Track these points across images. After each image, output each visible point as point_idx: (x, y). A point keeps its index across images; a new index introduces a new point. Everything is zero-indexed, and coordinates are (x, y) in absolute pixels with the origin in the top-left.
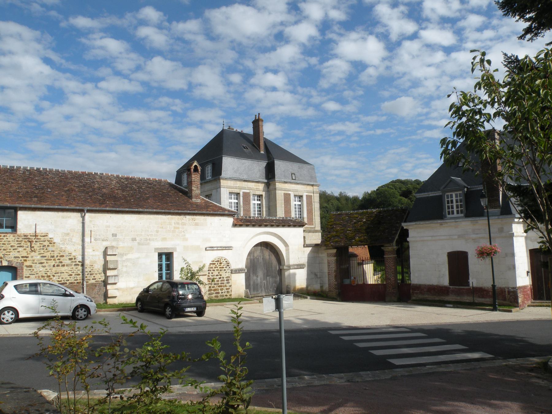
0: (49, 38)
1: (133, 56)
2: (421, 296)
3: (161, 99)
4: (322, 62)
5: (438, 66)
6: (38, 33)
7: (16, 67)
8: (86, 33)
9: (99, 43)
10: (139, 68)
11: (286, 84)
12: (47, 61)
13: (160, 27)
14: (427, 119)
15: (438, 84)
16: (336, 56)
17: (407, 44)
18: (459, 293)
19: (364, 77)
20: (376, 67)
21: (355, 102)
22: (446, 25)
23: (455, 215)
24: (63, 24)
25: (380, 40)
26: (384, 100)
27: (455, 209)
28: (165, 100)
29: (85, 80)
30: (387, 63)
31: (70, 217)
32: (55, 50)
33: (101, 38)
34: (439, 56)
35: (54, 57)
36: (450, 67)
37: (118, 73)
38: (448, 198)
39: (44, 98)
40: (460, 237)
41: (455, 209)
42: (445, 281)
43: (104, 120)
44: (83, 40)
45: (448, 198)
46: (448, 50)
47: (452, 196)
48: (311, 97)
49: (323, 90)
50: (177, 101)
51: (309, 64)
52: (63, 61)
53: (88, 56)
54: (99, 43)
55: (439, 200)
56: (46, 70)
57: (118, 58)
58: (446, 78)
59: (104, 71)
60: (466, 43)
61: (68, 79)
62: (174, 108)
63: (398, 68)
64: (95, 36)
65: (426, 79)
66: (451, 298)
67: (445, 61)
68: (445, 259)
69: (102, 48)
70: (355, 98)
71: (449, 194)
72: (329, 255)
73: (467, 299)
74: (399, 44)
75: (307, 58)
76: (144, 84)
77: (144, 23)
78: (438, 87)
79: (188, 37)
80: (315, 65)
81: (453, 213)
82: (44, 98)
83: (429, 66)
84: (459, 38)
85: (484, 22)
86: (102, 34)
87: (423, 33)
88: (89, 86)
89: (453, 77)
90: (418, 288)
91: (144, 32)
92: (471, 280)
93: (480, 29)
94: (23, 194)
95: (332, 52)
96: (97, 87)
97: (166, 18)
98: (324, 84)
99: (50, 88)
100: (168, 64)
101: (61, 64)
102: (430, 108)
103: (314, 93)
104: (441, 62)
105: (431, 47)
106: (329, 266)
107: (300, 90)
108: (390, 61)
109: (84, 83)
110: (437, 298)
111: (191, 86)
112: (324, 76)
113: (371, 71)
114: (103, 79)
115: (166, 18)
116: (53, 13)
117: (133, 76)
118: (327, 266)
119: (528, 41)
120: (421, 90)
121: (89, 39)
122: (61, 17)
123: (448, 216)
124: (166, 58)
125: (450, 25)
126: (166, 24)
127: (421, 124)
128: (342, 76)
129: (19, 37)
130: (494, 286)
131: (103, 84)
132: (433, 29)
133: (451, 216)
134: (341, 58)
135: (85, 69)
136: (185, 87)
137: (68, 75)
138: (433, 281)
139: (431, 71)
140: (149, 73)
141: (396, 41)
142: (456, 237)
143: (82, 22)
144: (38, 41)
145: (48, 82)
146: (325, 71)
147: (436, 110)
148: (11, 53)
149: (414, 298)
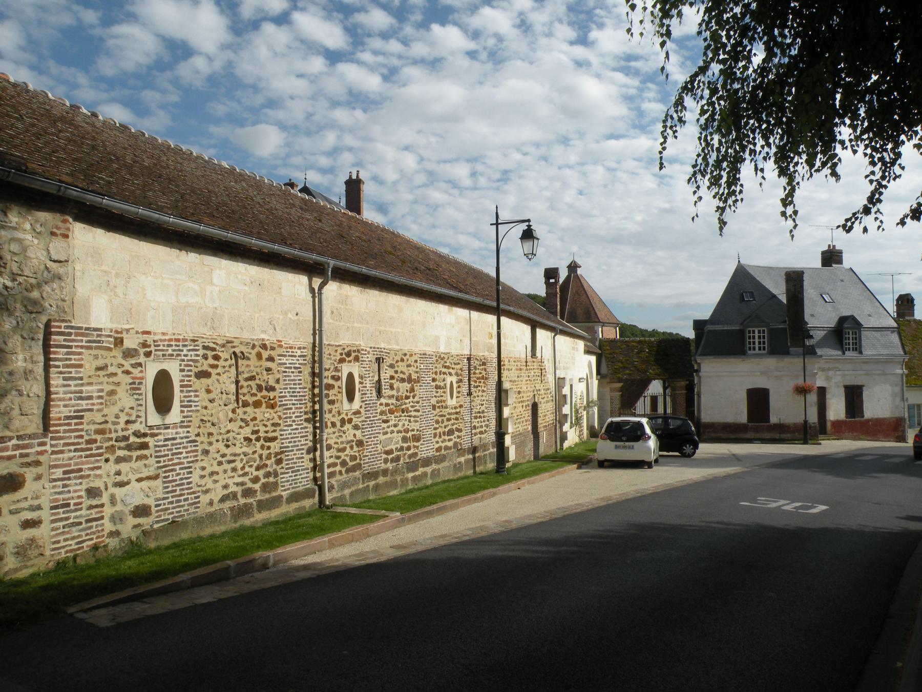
2: (713, 435)
4: (108, 21)
5: (313, 79)
11: (22, 49)
14: (286, 165)
15: (310, 110)
16: (132, 18)
17: (269, 28)
18: (757, 430)
19: (184, 70)
20: (210, 59)
21: (161, 113)
22: (335, 14)
23: (757, 350)
25: (222, 12)
26: (216, 121)
27: (757, 346)
30: (229, 55)
31: (505, 334)
34: (317, 64)
36: (333, 86)
38: (750, 333)
40: (763, 373)
41: (757, 346)
42: (743, 418)
45: (750, 333)
46: (333, 57)
47: (754, 332)
48: (76, 86)
49: (102, 79)
51: (79, 20)
55: (741, 334)
58: (323, 104)
60: (362, 51)
63: (246, 69)
65: (292, 98)
66: (749, 435)
67: (327, 73)
68: (745, 395)
70: (163, 107)
71: (751, 329)
72: (612, 390)
73: (767, 435)
74: (256, 25)
75: (75, 7)
78: (309, 116)
80: (92, 26)
81: (754, 349)
83: (300, 76)
84: (351, 40)
85: (392, 26)
87: (297, 17)
89: (335, 104)
90: (712, 426)
92: (771, 419)
93: (385, 36)
95: (129, 8)
98: (106, 67)
103: (83, 80)
104: (320, 73)
105: (310, 47)
106: (611, 402)
107: (53, 66)
108: (235, 52)
110: (733, 436)
112: (108, 54)
113: (199, 62)
118: (609, 403)
119: (808, 179)
120: (281, 115)
123: (749, 352)
125: (341, 16)
127: (274, 172)
128: (143, 60)
130: (806, 421)
132: (314, 15)
133: (752, 352)
134: (143, 24)
138: (730, 418)
139: (300, 86)
141: (249, 20)
142: (759, 373)
146: (111, 42)
147: (301, 153)
149: (705, 437)
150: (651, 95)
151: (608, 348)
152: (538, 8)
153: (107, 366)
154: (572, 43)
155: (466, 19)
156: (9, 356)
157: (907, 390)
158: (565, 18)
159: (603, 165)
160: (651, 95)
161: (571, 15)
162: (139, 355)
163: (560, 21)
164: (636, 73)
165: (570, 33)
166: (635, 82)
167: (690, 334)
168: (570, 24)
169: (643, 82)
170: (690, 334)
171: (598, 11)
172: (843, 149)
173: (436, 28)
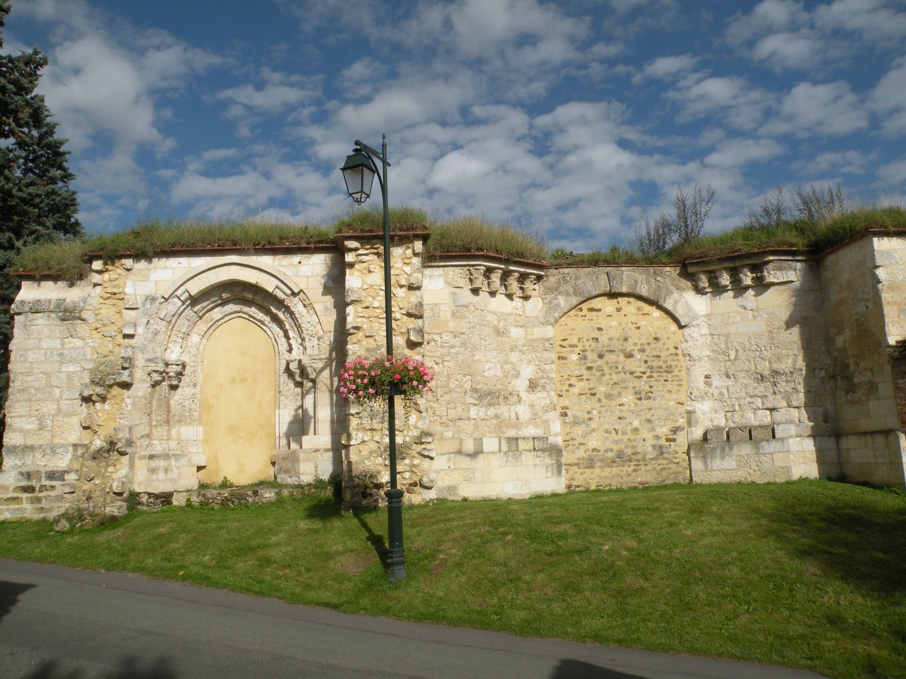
0: (618, 107)
1: (755, 95)
3: (819, 159)
6: (602, 106)
7: (588, 165)
8: (672, 82)
9: (697, 91)
10: (769, 114)
12: (624, 144)
13: (793, 28)
24: (637, 79)
28: (825, 160)
29: (684, 160)
32: (629, 122)
33: (698, 82)
35: (632, 134)
37: (735, 134)
39: (632, 202)
43: (725, 217)
44: (672, 95)
50: (851, 155)
52: (647, 138)
53: (683, 118)
54: (697, 91)
56: (625, 158)
57: (730, 107)
59: (710, 136)
61: (660, 164)
62: (846, 170)
64: (688, 82)
69: (702, 97)
76: (785, 139)
77: (770, 30)
79: (854, 23)
82: (632, 202)
86: (696, 76)
88: (692, 167)
91: (768, 46)
94: (294, 452)
96: (704, 165)
97: (800, 5)
99: (635, 185)
100: (823, 92)
101: (644, 143)
102: (109, 392)
109: (684, 164)
111: (875, 120)
114: (711, 150)
115: (800, 5)
116: (621, 69)
117: (763, 131)
121: (680, 90)
122: (631, 69)
124: (815, 83)
126: (805, 16)
129: (583, 121)
131: (713, 158)
135: (679, 140)
136: (864, 124)
137: (657, 157)
140: (790, 118)
143: (664, 66)
144: (607, 117)
145: (632, 177)
148: (576, 148)
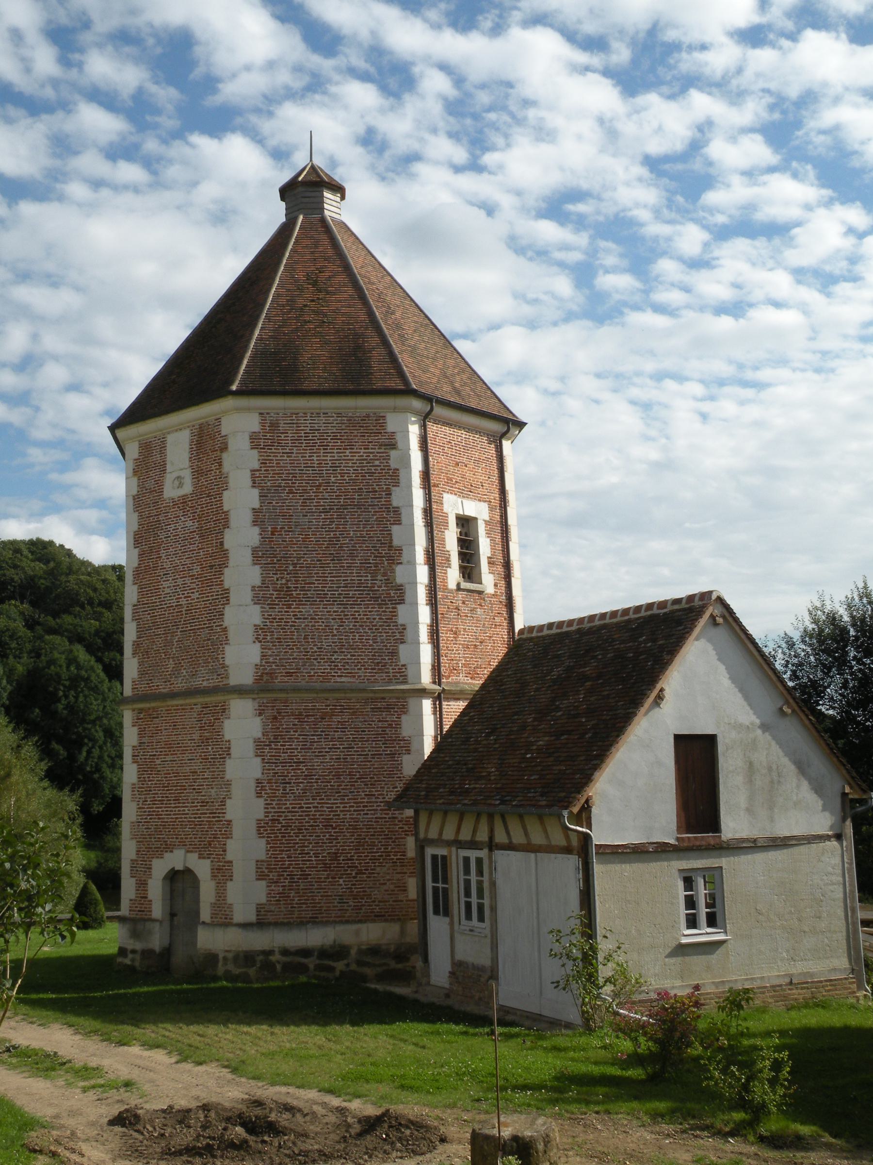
150: (610, 260)
151: (493, 770)
152: (392, 109)
153: (447, 913)
154: (458, 169)
155: (266, 126)
156: (337, 943)
157: (600, 862)
158: (441, 124)
159: (256, 137)
160: (610, 260)
161: (451, 119)
162: (279, 952)
163: (434, 131)
164: (580, 223)
165: (460, 155)
166: (582, 239)
167: (57, 545)
168: (453, 135)
169: (592, 238)
170: (57, 545)
171: (492, 116)
172: (855, 279)
173: (203, 143)
